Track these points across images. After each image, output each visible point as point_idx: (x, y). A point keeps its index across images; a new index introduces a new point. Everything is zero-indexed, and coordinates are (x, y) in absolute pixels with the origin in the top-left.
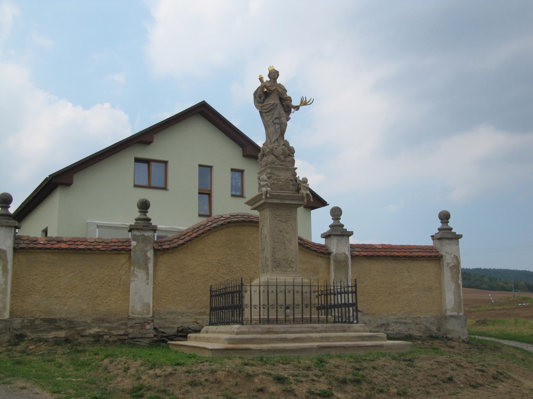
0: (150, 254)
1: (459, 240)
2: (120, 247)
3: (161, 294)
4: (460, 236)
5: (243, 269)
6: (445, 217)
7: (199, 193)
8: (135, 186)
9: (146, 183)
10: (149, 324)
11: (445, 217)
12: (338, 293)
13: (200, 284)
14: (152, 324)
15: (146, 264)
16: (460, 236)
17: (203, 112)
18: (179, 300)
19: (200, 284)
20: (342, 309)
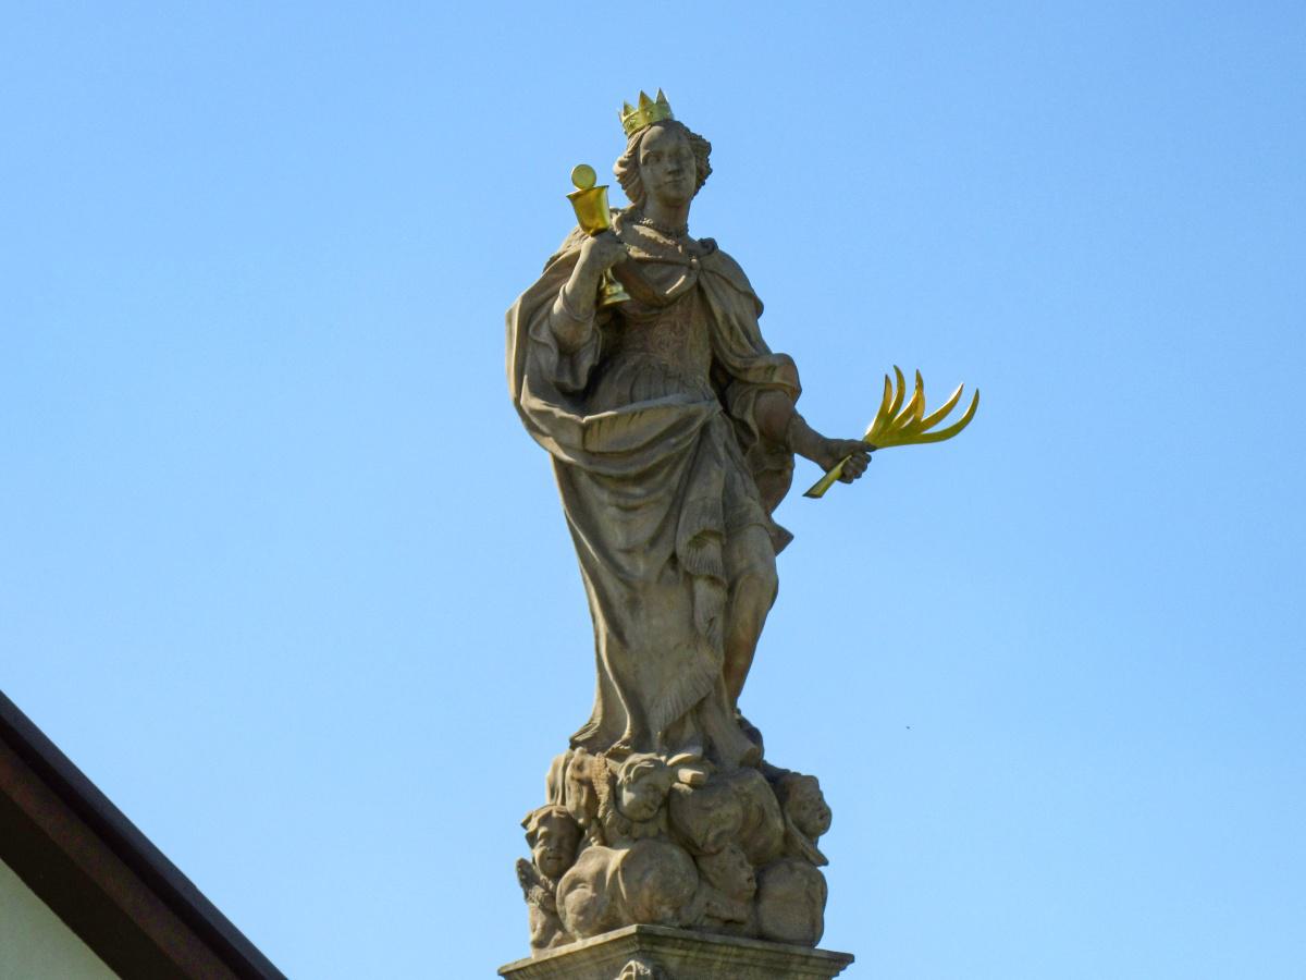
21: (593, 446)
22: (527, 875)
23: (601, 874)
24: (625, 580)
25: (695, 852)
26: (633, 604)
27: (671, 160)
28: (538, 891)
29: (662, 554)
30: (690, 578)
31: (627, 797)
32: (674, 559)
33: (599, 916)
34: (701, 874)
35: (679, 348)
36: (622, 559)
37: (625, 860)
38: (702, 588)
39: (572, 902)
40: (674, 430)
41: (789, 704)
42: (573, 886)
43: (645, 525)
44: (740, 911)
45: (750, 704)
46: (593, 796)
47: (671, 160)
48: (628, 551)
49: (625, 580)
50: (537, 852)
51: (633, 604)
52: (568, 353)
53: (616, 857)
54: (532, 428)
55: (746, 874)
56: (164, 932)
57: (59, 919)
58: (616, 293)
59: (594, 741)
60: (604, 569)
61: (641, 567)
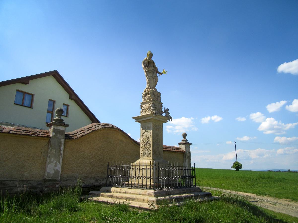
0: (63, 141)
1: (191, 145)
2: (44, 135)
3: (65, 165)
4: (191, 144)
5: (109, 153)
6: (185, 135)
7: (47, 112)
8: (15, 104)
9: (21, 104)
10: (58, 184)
11: (185, 135)
12: (184, 170)
13: (87, 160)
14: (59, 184)
15: (60, 147)
16: (191, 144)
17: (55, 75)
18: (75, 169)
19: (87, 160)
20: (183, 180)
21: (149, 70)
22: (143, 97)
23: (149, 96)
24: (150, 79)
25: (154, 95)
26: (150, 80)
27: (151, 55)
28: (143, 98)
29: (152, 77)
30: (154, 79)
31: (151, 91)
32: (153, 77)
33: (149, 99)
34: (155, 97)
35: (152, 65)
36: (150, 77)
37: (151, 96)
38: (155, 79)
39: (146, 98)
40: (153, 70)
41: (158, 88)
42: (147, 97)
43: (151, 75)
44: (157, 100)
45: (156, 87)
46: (148, 91)
47: (151, 55)
48: (150, 77)
49: (150, 79)
50: (144, 95)
51: (150, 80)
52: (146, 65)
53: (150, 95)
54: (144, 69)
55: (157, 97)
56: (94, 118)
57: (198, 168)
58: (149, 61)
59: (148, 88)
60: (63, 145)
61: (151, 78)
